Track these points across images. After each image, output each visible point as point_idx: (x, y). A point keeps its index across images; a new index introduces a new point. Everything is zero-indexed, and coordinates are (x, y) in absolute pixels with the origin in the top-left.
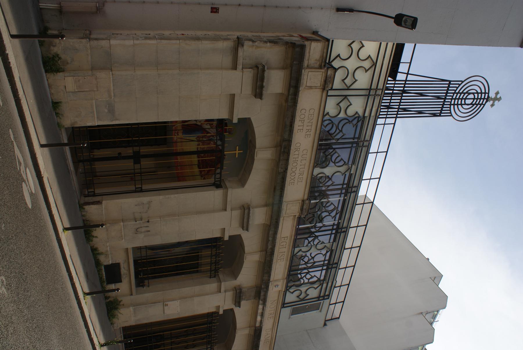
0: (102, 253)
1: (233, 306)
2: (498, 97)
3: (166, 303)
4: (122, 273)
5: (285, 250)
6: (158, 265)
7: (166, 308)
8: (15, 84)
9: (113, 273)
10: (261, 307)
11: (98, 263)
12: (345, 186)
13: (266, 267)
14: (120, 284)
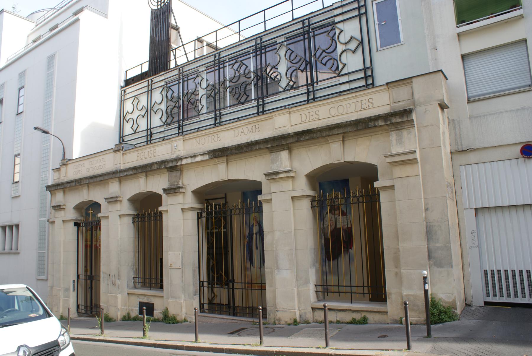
0: (129, 314)
4: (147, 301)
6: (151, 270)
9: (147, 308)
10: (184, 162)
11: (135, 319)
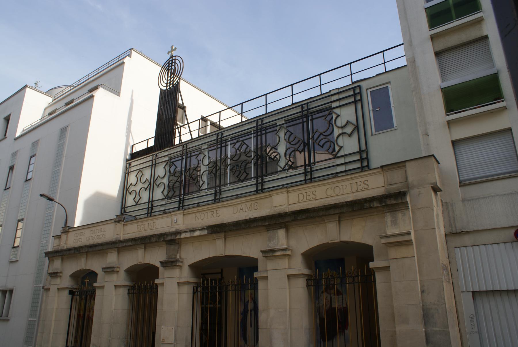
1: (161, 269)
2: (173, 48)
3: (161, 340)
5: (147, 223)
7: (166, 341)
10: (183, 236)
12: (189, 155)
13: (145, 242)
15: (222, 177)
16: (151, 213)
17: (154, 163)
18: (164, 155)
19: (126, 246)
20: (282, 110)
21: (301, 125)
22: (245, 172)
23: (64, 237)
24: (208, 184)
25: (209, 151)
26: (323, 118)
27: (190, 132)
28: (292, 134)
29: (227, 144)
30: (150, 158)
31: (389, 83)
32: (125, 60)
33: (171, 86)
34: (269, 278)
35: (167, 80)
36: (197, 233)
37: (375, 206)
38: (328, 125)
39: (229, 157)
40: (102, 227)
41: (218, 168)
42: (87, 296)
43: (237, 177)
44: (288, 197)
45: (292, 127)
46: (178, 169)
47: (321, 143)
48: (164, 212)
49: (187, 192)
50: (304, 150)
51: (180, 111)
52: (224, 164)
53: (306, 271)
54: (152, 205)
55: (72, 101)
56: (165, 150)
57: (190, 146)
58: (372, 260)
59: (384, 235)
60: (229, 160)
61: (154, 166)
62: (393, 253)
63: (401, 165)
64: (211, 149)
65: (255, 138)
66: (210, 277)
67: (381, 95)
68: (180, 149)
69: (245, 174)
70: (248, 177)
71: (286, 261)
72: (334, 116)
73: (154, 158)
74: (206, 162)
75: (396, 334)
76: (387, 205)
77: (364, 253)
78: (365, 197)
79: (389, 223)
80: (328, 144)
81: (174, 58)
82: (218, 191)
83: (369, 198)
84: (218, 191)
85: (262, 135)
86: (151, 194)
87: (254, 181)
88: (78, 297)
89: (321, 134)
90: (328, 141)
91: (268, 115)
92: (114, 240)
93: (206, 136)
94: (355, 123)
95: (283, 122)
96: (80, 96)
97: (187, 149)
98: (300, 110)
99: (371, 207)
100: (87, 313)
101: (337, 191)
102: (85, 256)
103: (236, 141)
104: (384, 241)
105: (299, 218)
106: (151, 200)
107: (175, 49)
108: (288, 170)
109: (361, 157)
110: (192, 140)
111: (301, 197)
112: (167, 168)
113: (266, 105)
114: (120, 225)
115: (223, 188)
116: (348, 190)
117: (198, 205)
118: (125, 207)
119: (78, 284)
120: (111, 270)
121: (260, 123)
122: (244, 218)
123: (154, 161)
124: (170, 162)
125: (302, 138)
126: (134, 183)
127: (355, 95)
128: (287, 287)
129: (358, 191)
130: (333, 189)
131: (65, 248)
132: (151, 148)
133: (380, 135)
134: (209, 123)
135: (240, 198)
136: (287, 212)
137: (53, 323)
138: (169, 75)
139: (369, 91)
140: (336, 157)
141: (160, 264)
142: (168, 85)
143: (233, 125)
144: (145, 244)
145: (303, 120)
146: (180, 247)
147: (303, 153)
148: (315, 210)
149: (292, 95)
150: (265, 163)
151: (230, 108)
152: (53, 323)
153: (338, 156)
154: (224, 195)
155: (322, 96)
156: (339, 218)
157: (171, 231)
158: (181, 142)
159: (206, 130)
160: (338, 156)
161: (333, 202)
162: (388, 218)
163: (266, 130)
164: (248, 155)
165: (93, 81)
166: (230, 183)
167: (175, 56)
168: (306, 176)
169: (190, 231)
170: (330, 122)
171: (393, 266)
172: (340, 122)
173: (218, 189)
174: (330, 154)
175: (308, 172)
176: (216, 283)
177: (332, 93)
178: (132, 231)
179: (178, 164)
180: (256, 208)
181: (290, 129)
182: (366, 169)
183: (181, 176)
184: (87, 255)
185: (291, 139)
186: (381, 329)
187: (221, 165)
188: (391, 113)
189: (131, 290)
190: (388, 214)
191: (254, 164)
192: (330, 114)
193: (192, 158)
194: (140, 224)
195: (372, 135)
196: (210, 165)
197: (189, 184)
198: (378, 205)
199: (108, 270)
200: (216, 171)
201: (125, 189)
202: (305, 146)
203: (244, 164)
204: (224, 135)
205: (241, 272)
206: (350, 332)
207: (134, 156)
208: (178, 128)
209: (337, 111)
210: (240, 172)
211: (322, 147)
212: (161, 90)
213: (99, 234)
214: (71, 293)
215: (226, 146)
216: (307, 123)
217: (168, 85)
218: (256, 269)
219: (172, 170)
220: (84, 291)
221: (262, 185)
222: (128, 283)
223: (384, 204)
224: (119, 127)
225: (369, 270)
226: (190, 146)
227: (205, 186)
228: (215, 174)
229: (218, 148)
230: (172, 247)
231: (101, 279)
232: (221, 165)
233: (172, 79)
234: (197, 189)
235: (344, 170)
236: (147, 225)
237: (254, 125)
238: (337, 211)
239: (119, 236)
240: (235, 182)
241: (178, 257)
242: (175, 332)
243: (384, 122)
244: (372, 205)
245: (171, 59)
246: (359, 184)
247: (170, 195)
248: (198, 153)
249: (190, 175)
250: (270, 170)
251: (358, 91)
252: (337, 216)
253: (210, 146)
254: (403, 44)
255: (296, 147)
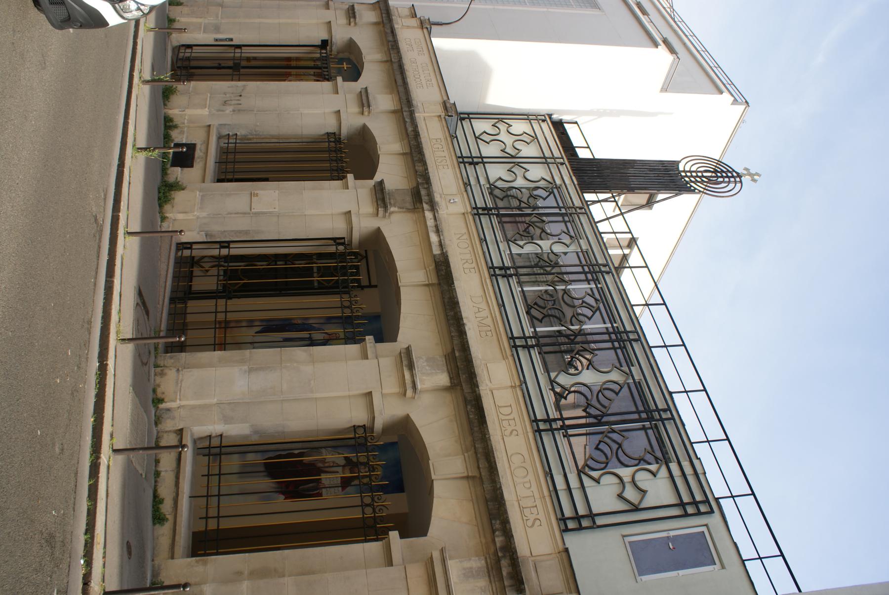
0: (176, 127)
1: (371, 183)
2: (756, 177)
5: (446, 154)
8: (112, 294)
10: (429, 215)
11: (167, 138)
12: (566, 219)
13: (415, 153)
14: (196, 530)
15: (533, 278)
16: (464, 163)
17: (549, 160)
18: (565, 176)
19: (405, 122)
20: (658, 375)
21: (634, 409)
22: (545, 316)
23: (414, 22)
24: (520, 255)
25: (577, 253)
26: (649, 448)
27: (608, 219)
28: (617, 394)
29: (592, 282)
30: (557, 154)
31: (723, 567)
32: (726, 95)
33: (687, 179)
34: (366, 361)
35: (696, 172)
36: (434, 238)
37: (497, 539)
38: (636, 456)
39: (569, 287)
40: (434, 81)
41: (548, 269)
42: (320, 68)
43: (536, 304)
44: (506, 388)
45: (629, 394)
46: (540, 203)
47: (602, 446)
48: (467, 184)
49: (504, 219)
50: (590, 415)
51: (642, 198)
52: (556, 279)
53: (379, 425)
54: (477, 163)
55: (644, 12)
56: (574, 178)
57: (583, 219)
58: (402, 536)
59: (447, 555)
60: (563, 287)
61: (544, 160)
62: (416, 573)
63: (572, 586)
64: (581, 255)
65: (605, 331)
66: (362, 264)
67: (698, 552)
68: (577, 203)
69: (540, 316)
70: (535, 322)
71: (396, 389)
72: (653, 467)
73: (558, 160)
74: (558, 249)
75: (279, 577)
76: (498, 561)
77: (414, 524)
78: (511, 520)
79: (467, 564)
80: (603, 459)
81: (738, 179)
82: (508, 272)
83: (510, 529)
84: (508, 272)
85: (612, 341)
86: (496, 160)
87: (529, 331)
88: (318, 55)
89: (620, 446)
90: (607, 458)
91: (648, 350)
92: (414, 103)
93: (604, 247)
94: (643, 506)
95: (636, 378)
96: (656, 25)
97: (578, 214)
98: (660, 407)
99: (494, 532)
100: (293, 71)
101: (520, 473)
102: (385, 59)
103: (598, 297)
104: (436, 555)
105: (469, 407)
106: (485, 160)
107: (754, 180)
108: (553, 389)
109: (583, 517)
110: (593, 224)
111: (507, 411)
112: (542, 184)
113: (665, 346)
114: (440, 110)
115: (514, 281)
116: (522, 492)
117: (483, 240)
118: (470, 119)
119: (338, 53)
120: (365, 102)
121: (632, 336)
122: (464, 315)
123: (553, 161)
124: (552, 188)
125: (609, 412)
126: (512, 130)
127: (695, 503)
128: (351, 393)
129: (522, 509)
130: (523, 465)
131: (396, 26)
132: (575, 154)
133: (625, 551)
134: (627, 251)
135: (500, 309)
136: (478, 387)
137: (276, 21)
138: (705, 174)
139: (704, 529)
140: (580, 472)
141: (379, 180)
142: (689, 174)
143: (625, 290)
144: (411, 153)
145: (642, 412)
146: (409, 210)
147: (584, 414)
148: (485, 435)
149: (686, 392)
150: (564, 348)
151: (656, 285)
152: (276, 21)
153: (582, 475)
154: (502, 282)
155: (688, 445)
156: (473, 477)
157: (435, 194)
158: (587, 204)
159: (614, 247)
160: (582, 475)
161: (499, 466)
162: (477, 563)
163: (620, 348)
164: (574, 319)
165: (685, 44)
166: (523, 291)
167: (741, 182)
168: (544, 421)
169: (437, 226)
170: (641, 460)
171: (394, 572)
172: (643, 478)
173: (512, 271)
174: (586, 461)
175: (551, 425)
176: (352, 274)
177: (695, 462)
178: (432, 132)
179: (551, 201)
180: (483, 334)
181: (625, 389)
182: (563, 527)
183: (530, 207)
184: (386, 61)
185: (607, 393)
186: (286, 551)
187: (553, 274)
188: (665, 571)
189: (333, 138)
190: (483, 562)
191: (559, 331)
192: (657, 460)
193: (563, 224)
194: (443, 143)
195: (624, 536)
196: (552, 257)
197: (516, 222)
198: (498, 545)
199: (364, 98)
200: (541, 267)
201: (501, 117)
202: (595, 417)
203: (557, 313)
204: (606, 276)
205: (376, 318)
206: (281, 502)
207: (559, 127)
208: (613, 197)
209: (663, 472)
210: (544, 308)
211: (597, 448)
212: (676, 163)
213: (422, 78)
214: (325, 44)
215: (588, 281)
216: (636, 422)
217: (689, 174)
218: (380, 338)
219: (540, 192)
220: (328, 62)
221: (523, 347)
222: (344, 131)
223: (500, 554)
224: (607, 95)
225: (385, 532)
226: (583, 219)
227: (515, 250)
228: (536, 266)
229: (583, 266)
230: (409, 199)
231: (348, 89)
232: (553, 274)
233: (698, 179)
234: (509, 236)
235: (558, 488)
236: (443, 154)
237: (629, 328)
238: (484, 473)
239: (421, 109)
240: (526, 301)
241: (392, 209)
242: (270, 213)
243: (649, 559)
244: (497, 533)
245: (735, 174)
246: (534, 510)
247: (497, 192)
248: (572, 234)
249: (533, 223)
250: (550, 358)
251: (703, 508)
252: (476, 474)
253: (585, 253)
254: (800, 591)
255: (594, 402)
